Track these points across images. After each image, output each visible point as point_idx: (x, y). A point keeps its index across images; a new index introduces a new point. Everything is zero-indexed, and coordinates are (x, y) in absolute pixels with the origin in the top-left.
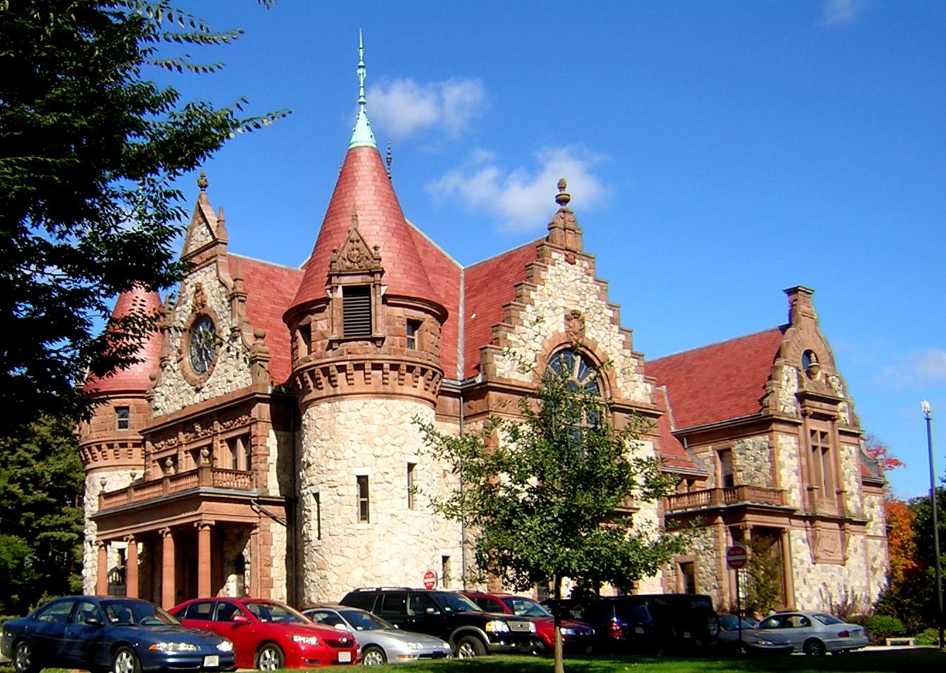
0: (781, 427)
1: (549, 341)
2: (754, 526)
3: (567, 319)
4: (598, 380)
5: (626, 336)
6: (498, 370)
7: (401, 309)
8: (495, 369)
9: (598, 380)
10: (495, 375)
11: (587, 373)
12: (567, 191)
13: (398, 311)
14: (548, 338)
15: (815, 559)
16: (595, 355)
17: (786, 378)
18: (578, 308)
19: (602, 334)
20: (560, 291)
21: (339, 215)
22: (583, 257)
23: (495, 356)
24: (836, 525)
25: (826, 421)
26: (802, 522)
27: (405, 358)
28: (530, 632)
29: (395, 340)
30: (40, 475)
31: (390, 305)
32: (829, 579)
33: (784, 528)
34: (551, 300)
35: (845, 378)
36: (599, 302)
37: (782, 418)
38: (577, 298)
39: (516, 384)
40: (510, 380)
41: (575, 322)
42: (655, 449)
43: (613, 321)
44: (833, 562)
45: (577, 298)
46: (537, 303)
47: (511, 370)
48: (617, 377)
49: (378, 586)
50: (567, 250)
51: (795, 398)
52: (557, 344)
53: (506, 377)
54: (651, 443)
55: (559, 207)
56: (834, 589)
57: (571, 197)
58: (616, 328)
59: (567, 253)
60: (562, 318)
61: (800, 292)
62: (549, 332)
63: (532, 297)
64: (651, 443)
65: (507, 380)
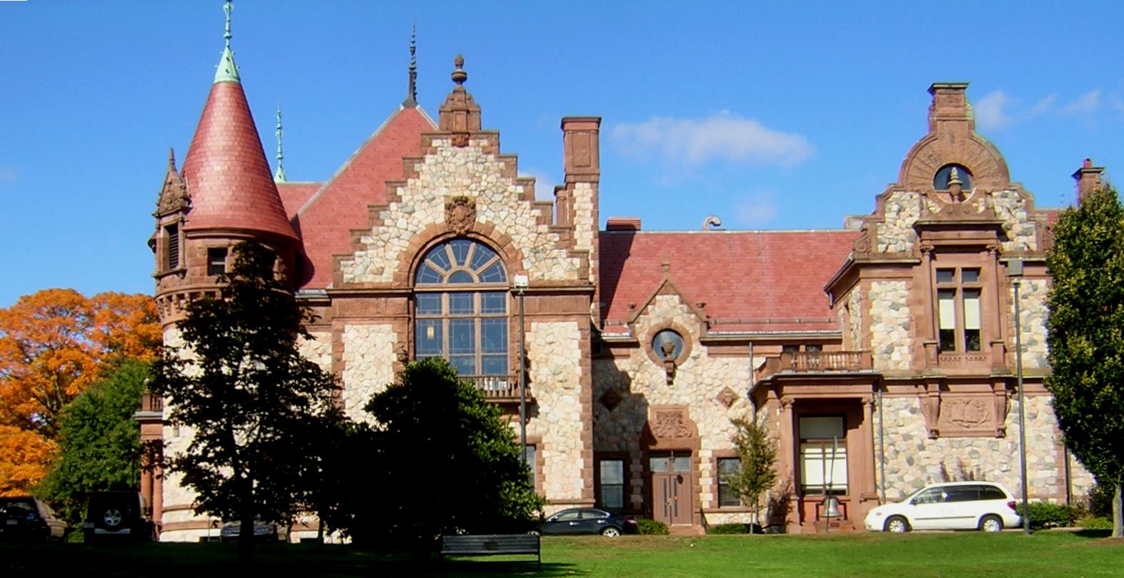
0: (877, 272)
1: (421, 235)
2: (796, 399)
3: (449, 207)
4: (501, 262)
5: (542, 209)
6: (345, 276)
7: (200, 240)
8: (342, 276)
9: (501, 262)
10: (342, 281)
11: (430, 270)
12: (464, 69)
13: (199, 243)
14: (418, 233)
15: (935, 434)
16: (491, 239)
17: (895, 208)
18: (466, 193)
19: (503, 215)
20: (441, 179)
21: (227, 148)
22: (481, 136)
23: (342, 262)
24: (987, 387)
25: (979, 252)
26: (913, 387)
27: (203, 285)
28: (241, 526)
29: (196, 270)
30: (90, 408)
31: (191, 238)
32: (967, 456)
33: (861, 398)
34: (426, 192)
35: (1027, 187)
36: (503, 180)
37: (872, 262)
38: (466, 182)
39: (371, 287)
40: (363, 284)
41: (459, 211)
42: (580, 329)
43: (522, 197)
44: (988, 434)
45: (466, 182)
46: (405, 199)
47: (364, 273)
48: (523, 258)
49: (580, 490)
50: (454, 133)
51: (913, 231)
52: (432, 237)
53: (357, 281)
54: (576, 323)
55: (456, 86)
56: (951, 469)
57: (468, 77)
58: (527, 204)
59: (454, 136)
60: (442, 208)
61: (938, 91)
62: (420, 226)
63: (399, 194)
64: (576, 323)
65: (358, 284)
